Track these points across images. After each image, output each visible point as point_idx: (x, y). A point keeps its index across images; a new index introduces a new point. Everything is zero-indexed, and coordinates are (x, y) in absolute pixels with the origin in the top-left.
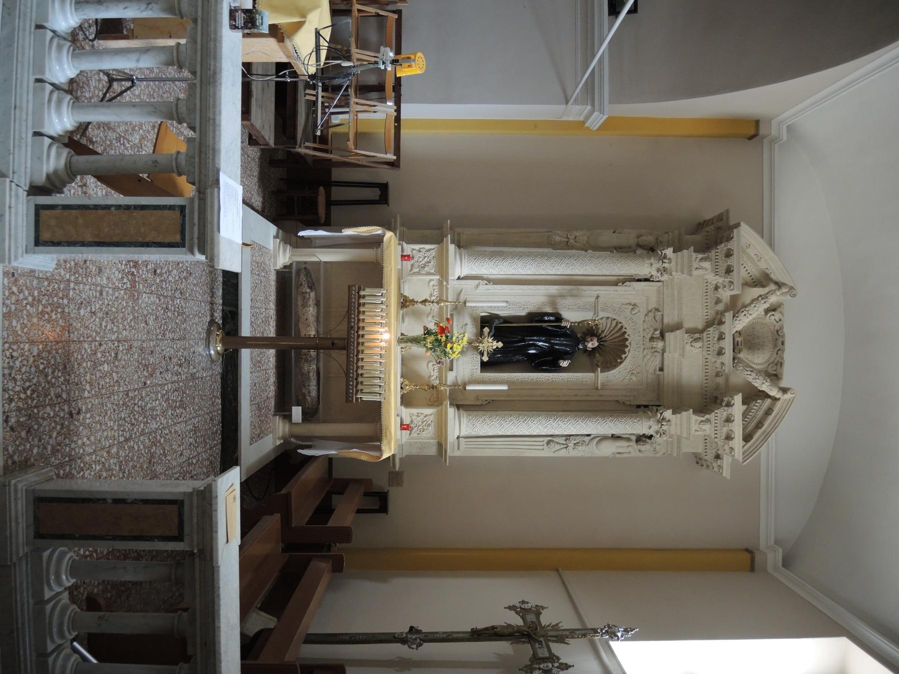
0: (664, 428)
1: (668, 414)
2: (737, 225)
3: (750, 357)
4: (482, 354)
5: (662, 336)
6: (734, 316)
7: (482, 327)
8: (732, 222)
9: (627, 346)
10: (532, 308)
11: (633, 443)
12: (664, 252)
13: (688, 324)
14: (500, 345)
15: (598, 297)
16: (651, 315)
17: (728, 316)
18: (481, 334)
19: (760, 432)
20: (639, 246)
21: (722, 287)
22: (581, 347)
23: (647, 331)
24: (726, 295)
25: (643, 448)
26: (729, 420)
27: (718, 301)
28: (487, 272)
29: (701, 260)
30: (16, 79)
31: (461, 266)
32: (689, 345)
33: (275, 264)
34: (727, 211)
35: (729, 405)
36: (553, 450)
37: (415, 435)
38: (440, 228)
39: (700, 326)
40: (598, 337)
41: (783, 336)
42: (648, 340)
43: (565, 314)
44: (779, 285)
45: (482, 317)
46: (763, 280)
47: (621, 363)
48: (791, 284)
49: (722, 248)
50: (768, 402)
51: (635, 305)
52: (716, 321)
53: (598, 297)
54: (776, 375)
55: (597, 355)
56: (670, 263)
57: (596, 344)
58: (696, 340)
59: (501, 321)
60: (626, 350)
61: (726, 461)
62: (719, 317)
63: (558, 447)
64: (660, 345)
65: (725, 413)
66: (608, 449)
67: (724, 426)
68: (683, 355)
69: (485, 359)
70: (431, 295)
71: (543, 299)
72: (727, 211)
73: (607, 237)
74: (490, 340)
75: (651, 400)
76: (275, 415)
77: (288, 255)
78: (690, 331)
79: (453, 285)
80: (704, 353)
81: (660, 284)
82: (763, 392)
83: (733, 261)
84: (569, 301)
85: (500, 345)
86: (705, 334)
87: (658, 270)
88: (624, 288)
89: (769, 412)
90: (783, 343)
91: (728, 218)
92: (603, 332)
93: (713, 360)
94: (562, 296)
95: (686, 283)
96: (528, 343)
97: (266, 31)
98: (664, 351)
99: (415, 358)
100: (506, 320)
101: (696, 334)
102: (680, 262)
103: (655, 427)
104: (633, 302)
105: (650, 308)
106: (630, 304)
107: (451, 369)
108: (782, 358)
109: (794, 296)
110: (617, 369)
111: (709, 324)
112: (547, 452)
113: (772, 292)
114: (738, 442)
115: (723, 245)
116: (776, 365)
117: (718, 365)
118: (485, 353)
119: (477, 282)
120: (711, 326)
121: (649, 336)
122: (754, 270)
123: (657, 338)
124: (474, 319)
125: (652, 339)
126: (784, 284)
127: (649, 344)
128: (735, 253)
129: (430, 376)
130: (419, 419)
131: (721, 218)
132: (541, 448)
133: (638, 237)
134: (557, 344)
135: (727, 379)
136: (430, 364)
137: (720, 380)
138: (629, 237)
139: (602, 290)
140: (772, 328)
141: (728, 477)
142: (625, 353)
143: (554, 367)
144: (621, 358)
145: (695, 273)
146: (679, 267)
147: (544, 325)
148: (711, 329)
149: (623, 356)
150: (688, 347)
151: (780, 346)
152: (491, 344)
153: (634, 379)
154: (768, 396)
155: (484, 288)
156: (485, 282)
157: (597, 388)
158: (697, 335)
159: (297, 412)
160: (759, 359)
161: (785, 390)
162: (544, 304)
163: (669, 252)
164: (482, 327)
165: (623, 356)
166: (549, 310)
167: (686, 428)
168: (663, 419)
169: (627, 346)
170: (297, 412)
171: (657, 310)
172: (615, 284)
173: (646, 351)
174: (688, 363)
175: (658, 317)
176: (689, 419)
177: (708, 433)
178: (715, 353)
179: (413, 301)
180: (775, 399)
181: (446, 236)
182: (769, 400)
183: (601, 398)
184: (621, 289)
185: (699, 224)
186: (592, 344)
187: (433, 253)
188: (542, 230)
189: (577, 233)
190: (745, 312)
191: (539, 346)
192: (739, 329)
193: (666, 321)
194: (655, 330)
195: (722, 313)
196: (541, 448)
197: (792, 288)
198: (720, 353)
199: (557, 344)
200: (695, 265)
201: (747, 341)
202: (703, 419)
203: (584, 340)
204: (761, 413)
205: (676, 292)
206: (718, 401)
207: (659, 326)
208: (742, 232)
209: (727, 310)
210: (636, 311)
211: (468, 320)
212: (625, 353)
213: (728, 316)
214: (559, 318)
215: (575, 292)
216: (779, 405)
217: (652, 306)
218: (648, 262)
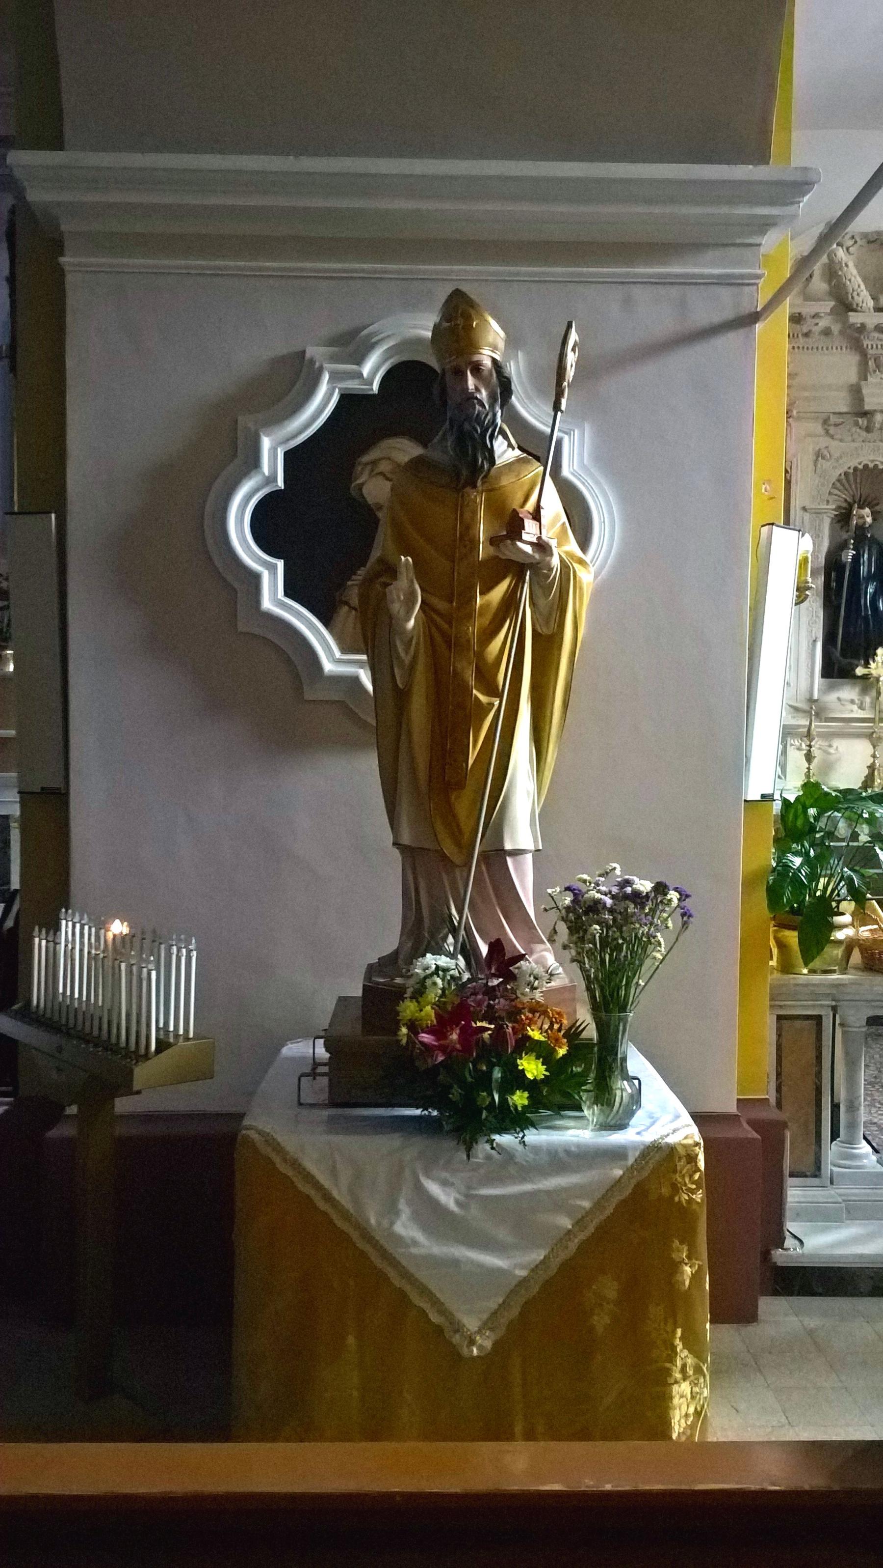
5: (865, 414)
6: (855, 311)
13: (852, 376)
15: (804, 509)
16: (832, 430)
23: (856, 436)
30: (835, 1107)
42: (870, 436)
52: (855, 337)
53: (804, 509)
70: (799, 749)
92: (846, 500)
104: (812, 457)
105: (822, 432)
106: (817, 459)
121: (864, 434)
124: (831, 688)
148: (866, 343)
171: (826, 422)
175: (833, 419)
179: (808, 775)
193: (844, 409)
194: (856, 424)
207: (850, 420)
210: (826, 453)
213: (854, 318)
217: (819, 429)
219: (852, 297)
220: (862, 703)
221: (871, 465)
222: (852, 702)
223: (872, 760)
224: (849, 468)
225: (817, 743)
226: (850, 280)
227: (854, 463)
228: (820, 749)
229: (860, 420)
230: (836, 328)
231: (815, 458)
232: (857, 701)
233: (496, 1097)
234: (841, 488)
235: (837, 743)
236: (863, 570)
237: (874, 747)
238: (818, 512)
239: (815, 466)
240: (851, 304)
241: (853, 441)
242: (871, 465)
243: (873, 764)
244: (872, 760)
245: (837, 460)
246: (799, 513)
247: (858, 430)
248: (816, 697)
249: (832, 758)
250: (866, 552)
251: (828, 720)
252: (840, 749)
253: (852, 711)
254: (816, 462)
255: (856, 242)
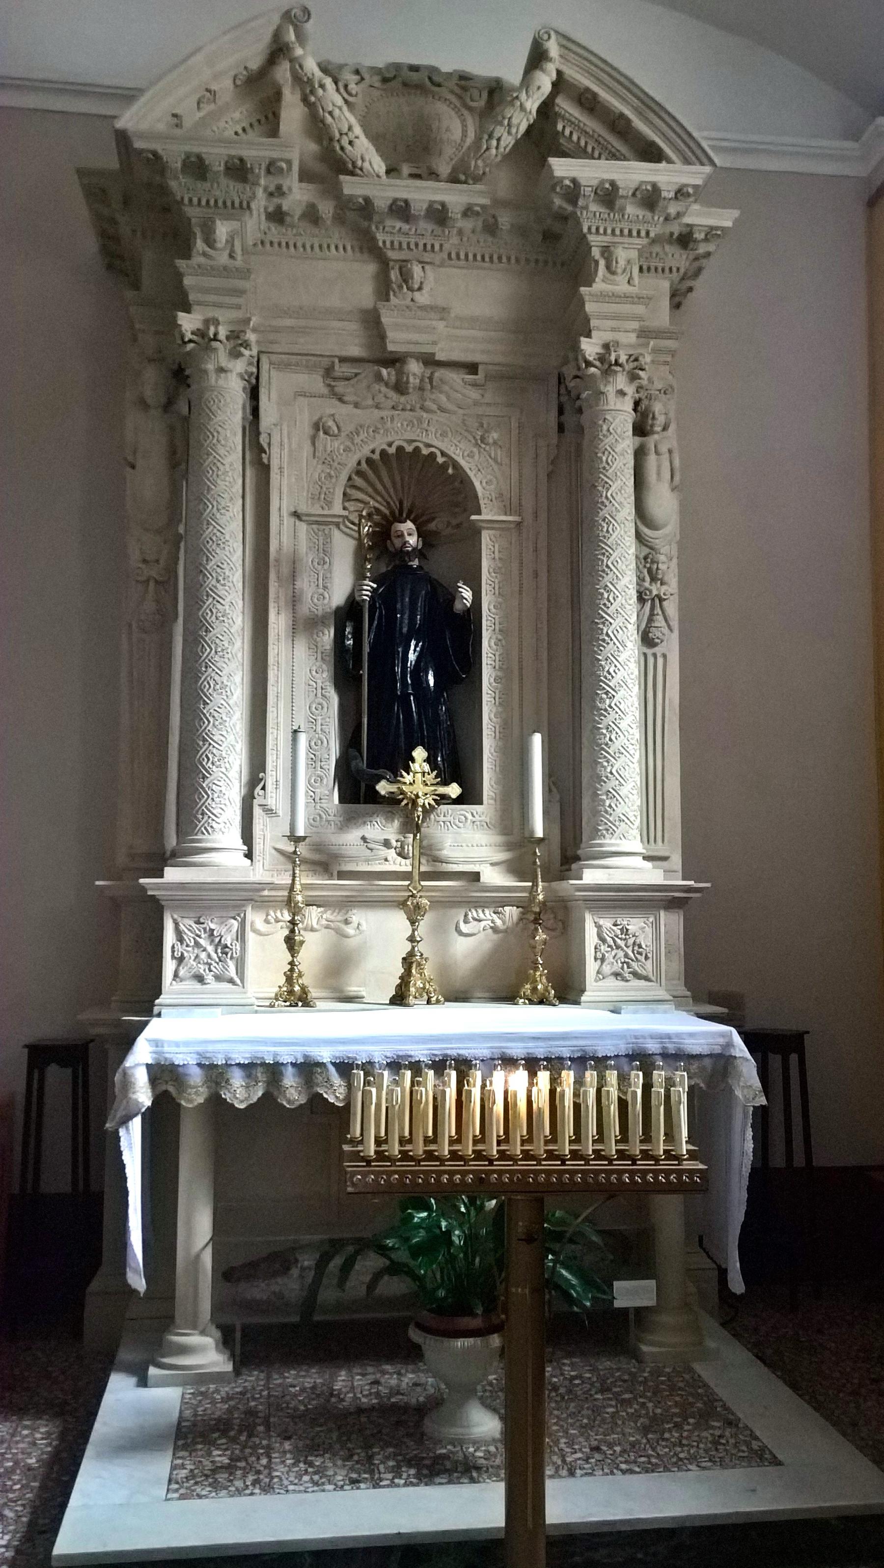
0: (623, 359)
1: (590, 347)
2: (123, 138)
3: (449, 151)
4: (443, 799)
5: (395, 361)
6: (352, 174)
7: (373, 798)
8: (112, 162)
9: (417, 450)
10: (324, 678)
11: (651, 441)
12: (188, 336)
14: (420, 753)
15: (296, 515)
17: (350, 186)
18: (392, 801)
19: (639, 124)
20: (168, 405)
21: (276, 200)
22: (415, 563)
23: (380, 398)
24: (298, 195)
25: (661, 420)
26: (608, 195)
27: (312, 215)
28: (237, 784)
29: (210, 242)
31: (223, 854)
32: (417, 295)
33: (218, 1378)
34: (81, 173)
35: (573, 192)
36: (666, 630)
37: (649, 965)
38: (115, 904)
39: (371, 268)
40: (390, 524)
41: (397, 67)
42: (403, 399)
43: (338, 597)
44: (278, 51)
45: (342, 800)
46: (261, 90)
47: (456, 465)
48: (276, 19)
49: (180, 186)
50: (564, 105)
51: (317, 426)
52: (359, 222)
53: (296, 515)
54: (491, 92)
55: (432, 526)
56: (217, 323)
57: (409, 525)
58: (406, 277)
59: (353, 752)
60: (425, 451)
61: (699, 217)
62: (351, 216)
63: (659, 621)
64: (414, 367)
65: (593, 207)
66: (664, 502)
67: (622, 210)
68: (442, 312)
69: (454, 790)
71: (301, 649)
72: (81, 173)
73: (148, 483)
74: (408, 778)
75: (553, 396)
76: (636, 1355)
77: (195, 1339)
78: (384, 289)
79: (264, 870)
80: (437, 258)
81: (264, 360)
82: (540, 110)
83: (216, 156)
84: (306, 585)
85: (420, 753)
86: (391, 254)
87: (235, 354)
88: (275, 451)
89: (588, 102)
90: (414, 68)
91: (101, 173)
93: (455, 240)
94: (294, 601)
95: (267, 297)
96: (407, 691)
97: (480, 367)
98: (429, 361)
99: (444, 969)
100: (350, 740)
101: (390, 278)
102: (212, 298)
103: (621, 381)
104: (308, 430)
105: (325, 391)
107: (475, 877)
108: (450, 75)
109: (307, 12)
110: (471, 474)
111: (369, 247)
112: (671, 645)
113: (296, 63)
114: (667, 176)
115: (173, 184)
116: (464, 89)
117: (467, 225)
118: (442, 790)
119: (257, 812)
120: (374, 239)
122: (237, 115)
123: (400, 373)
124: (349, 821)
125: (400, 388)
126: (277, 35)
127: (413, 398)
128: (196, 150)
129: (495, 929)
130: (609, 957)
131: (95, 186)
132: (660, 661)
133: (143, 404)
134: (412, 619)
135: (504, 204)
136: (464, 928)
137: (505, 220)
138: (146, 433)
139: (281, 504)
140: (376, 93)
141: (736, 213)
142: (432, 456)
143: (467, 625)
144: (444, 467)
145: (239, 261)
146: (227, 300)
147: (366, 649)
148: (380, 237)
149: (440, 460)
150: (422, 298)
151: (422, 76)
152: (419, 777)
153: (495, 435)
154: (546, 109)
155: (274, 795)
156: (258, 790)
157: (519, 524)
158: (394, 275)
159: (630, 1294)
160: (454, 128)
161: (537, 57)
162: (314, 646)
163: (188, 323)
164: (373, 798)
165: (440, 460)
166: (328, 636)
167: (619, 306)
168: (602, 359)
169: (417, 450)
170: (630, 1294)
171: (328, 372)
172: (263, 470)
173: (428, 404)
174: (461, 304)
176: (603, 297)
177: (634, 254)
178: (438, 230)
180: (560, 84)
181: (143, 889)
182: (559, 100)
183: (543, 516)
184: (276, 458)
185: (110, 267)
186: (409, 535)
187: (186, 924)
188: (125, 646)
189: (134, 555)
190: (345, 142)
191: (418, 660)
192: (384, 169)
193: (355, 350)
194: (379, 378)
195: (344, 204)
196: (660, 661)
197: (287, 16)
198: (439, 215)
199: (412, 619)
200: (223, 259)
201: (412, 151)
202: (602, 263)
203: (402, 554)
204: (591, 124)
205: (288, 322)
206: (557, 227)
208: (144, 126)
209: (334, 192)
210: (330, 423)
211: (352, 838)
212: (432, 456)
213: (350, 186)
214: (350, 612)
215: (285, 570)
216: (573, 74)
217: (317, 383)
218: (213, 377)
219: (342, 148)
220: (402, 847)
221: (409, 449)
222: (387, 844)
223: (408, 946)
224: (373, 452)
225: (313, 915)
226: (330, 113)
227: (379, 443)
228: (327, 927)
229: (384, 372)
230: (326, 209)
231: (311, 432)
232: (394, 844)
233: (477, 1260)
234: (370, 490)
235: (358, 916)
236: (403, 618)
237: (413, 923)
238: (320, 523)
239: (313, 444)
240: (345, 163)
241: (377, 407)
242: (409, 449)
243: (411, 954)
244: (408, 946)
245: (350, 437)
246: (288, 521)
247: (383, 389)
248: (301, 832)
249: (352, 943)
250: (408, 593)
251: (342, 875)
252: (364, 927)
253: (386, 860)
254: (313, 439)
255: (362, 79)
